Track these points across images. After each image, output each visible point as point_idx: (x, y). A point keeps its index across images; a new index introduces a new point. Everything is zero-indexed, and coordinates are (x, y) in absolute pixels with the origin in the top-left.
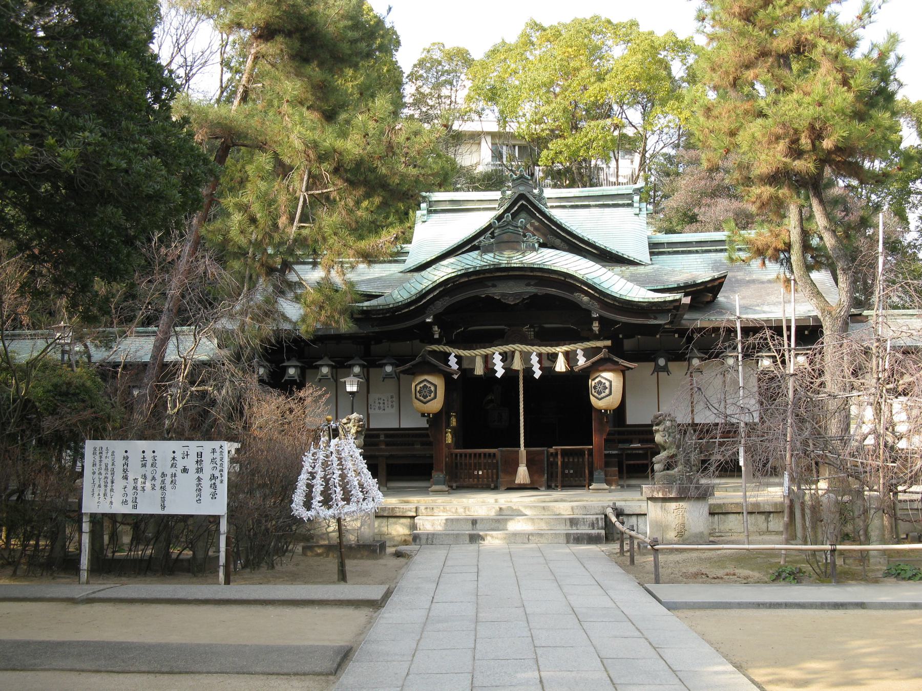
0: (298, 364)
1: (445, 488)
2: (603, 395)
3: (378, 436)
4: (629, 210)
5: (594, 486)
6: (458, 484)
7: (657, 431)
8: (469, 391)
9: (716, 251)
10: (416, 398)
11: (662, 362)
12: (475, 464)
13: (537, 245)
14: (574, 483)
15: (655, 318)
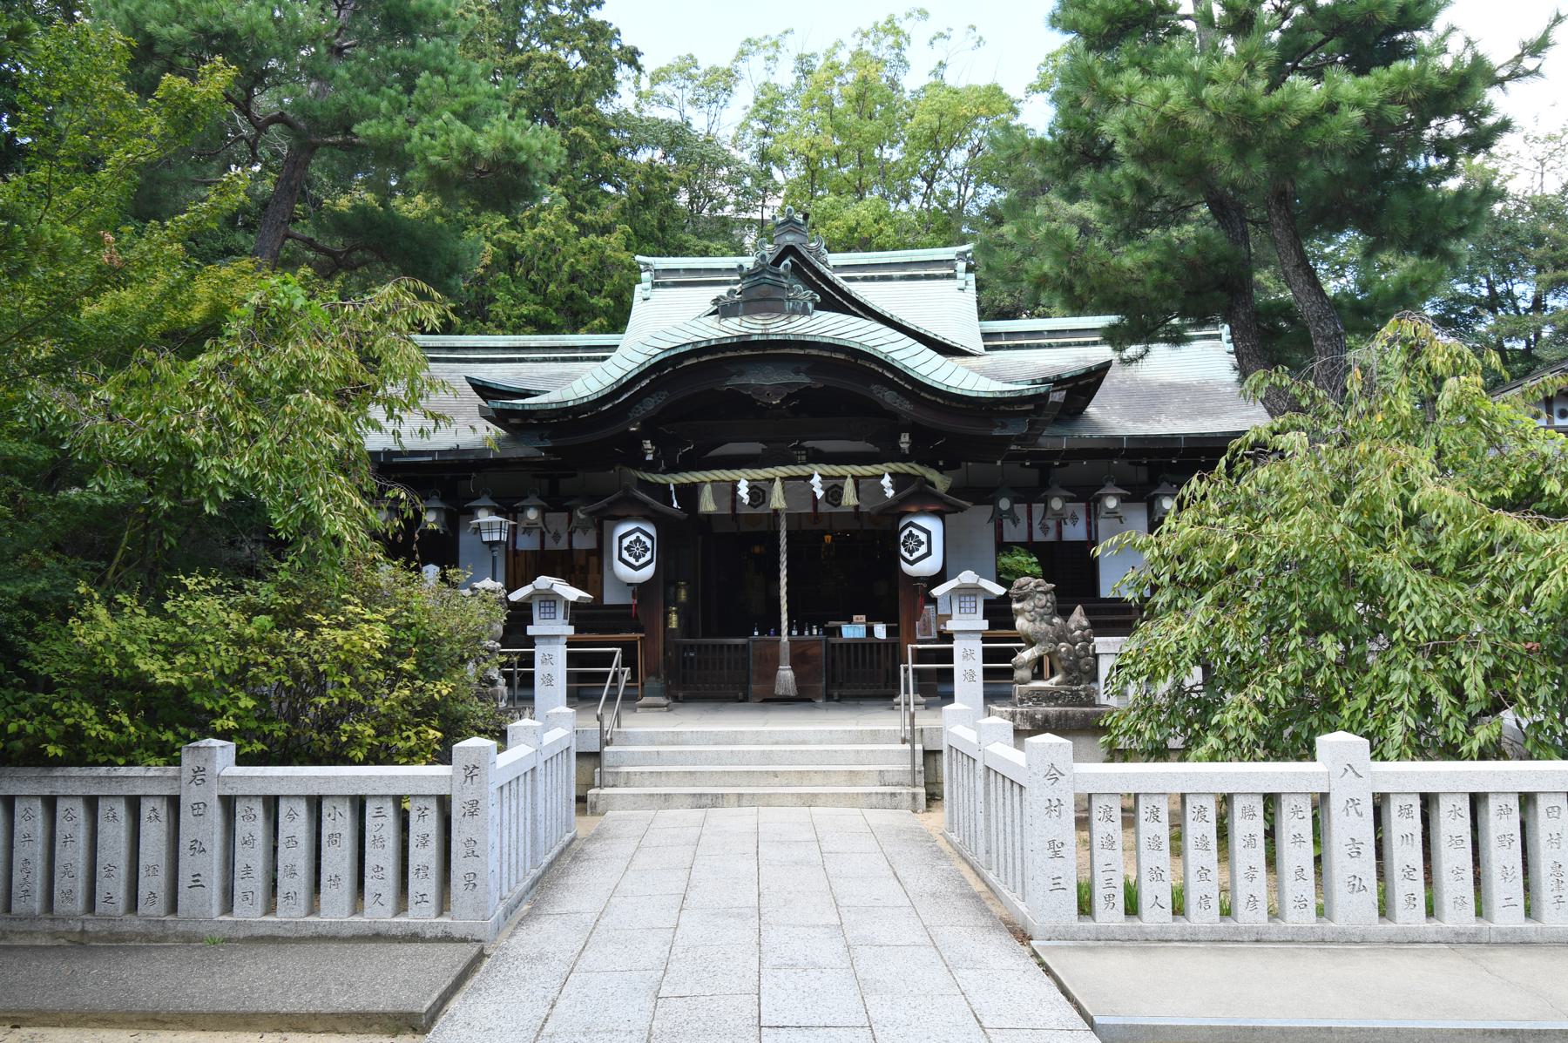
0: (439, 505)
1: (662, 700)
4: (951, 282)
7: (1021, 612)
9: (1079, 344)
10: (621, 559)
11: (1004, 504)
13: (810, 305)
15: (1004, 426)
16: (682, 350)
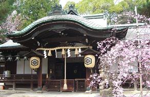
8: (55, 62)
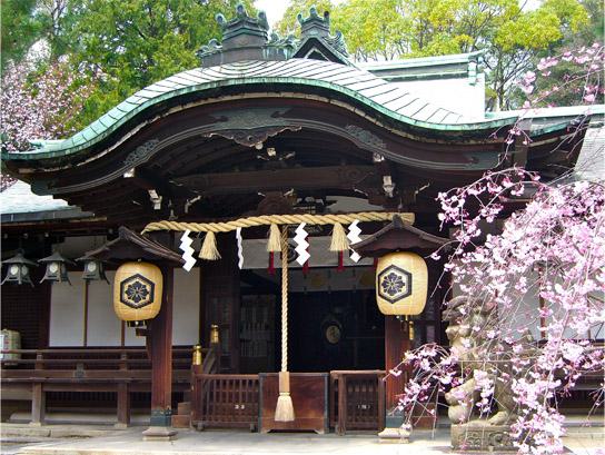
2: (398, 294)
3: (119, 356)
4: (465, 80)
5: (388, 431)
6: (206, 423)
8: (232, 288)
10: (122, 300)
12: (231, 396)
14: (368, 424)
16: (166, 98)
